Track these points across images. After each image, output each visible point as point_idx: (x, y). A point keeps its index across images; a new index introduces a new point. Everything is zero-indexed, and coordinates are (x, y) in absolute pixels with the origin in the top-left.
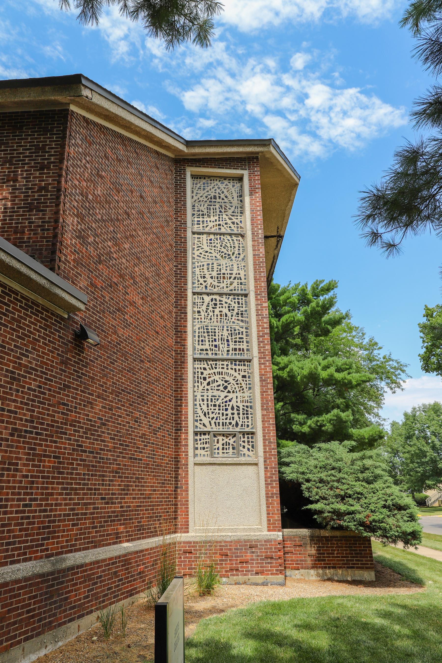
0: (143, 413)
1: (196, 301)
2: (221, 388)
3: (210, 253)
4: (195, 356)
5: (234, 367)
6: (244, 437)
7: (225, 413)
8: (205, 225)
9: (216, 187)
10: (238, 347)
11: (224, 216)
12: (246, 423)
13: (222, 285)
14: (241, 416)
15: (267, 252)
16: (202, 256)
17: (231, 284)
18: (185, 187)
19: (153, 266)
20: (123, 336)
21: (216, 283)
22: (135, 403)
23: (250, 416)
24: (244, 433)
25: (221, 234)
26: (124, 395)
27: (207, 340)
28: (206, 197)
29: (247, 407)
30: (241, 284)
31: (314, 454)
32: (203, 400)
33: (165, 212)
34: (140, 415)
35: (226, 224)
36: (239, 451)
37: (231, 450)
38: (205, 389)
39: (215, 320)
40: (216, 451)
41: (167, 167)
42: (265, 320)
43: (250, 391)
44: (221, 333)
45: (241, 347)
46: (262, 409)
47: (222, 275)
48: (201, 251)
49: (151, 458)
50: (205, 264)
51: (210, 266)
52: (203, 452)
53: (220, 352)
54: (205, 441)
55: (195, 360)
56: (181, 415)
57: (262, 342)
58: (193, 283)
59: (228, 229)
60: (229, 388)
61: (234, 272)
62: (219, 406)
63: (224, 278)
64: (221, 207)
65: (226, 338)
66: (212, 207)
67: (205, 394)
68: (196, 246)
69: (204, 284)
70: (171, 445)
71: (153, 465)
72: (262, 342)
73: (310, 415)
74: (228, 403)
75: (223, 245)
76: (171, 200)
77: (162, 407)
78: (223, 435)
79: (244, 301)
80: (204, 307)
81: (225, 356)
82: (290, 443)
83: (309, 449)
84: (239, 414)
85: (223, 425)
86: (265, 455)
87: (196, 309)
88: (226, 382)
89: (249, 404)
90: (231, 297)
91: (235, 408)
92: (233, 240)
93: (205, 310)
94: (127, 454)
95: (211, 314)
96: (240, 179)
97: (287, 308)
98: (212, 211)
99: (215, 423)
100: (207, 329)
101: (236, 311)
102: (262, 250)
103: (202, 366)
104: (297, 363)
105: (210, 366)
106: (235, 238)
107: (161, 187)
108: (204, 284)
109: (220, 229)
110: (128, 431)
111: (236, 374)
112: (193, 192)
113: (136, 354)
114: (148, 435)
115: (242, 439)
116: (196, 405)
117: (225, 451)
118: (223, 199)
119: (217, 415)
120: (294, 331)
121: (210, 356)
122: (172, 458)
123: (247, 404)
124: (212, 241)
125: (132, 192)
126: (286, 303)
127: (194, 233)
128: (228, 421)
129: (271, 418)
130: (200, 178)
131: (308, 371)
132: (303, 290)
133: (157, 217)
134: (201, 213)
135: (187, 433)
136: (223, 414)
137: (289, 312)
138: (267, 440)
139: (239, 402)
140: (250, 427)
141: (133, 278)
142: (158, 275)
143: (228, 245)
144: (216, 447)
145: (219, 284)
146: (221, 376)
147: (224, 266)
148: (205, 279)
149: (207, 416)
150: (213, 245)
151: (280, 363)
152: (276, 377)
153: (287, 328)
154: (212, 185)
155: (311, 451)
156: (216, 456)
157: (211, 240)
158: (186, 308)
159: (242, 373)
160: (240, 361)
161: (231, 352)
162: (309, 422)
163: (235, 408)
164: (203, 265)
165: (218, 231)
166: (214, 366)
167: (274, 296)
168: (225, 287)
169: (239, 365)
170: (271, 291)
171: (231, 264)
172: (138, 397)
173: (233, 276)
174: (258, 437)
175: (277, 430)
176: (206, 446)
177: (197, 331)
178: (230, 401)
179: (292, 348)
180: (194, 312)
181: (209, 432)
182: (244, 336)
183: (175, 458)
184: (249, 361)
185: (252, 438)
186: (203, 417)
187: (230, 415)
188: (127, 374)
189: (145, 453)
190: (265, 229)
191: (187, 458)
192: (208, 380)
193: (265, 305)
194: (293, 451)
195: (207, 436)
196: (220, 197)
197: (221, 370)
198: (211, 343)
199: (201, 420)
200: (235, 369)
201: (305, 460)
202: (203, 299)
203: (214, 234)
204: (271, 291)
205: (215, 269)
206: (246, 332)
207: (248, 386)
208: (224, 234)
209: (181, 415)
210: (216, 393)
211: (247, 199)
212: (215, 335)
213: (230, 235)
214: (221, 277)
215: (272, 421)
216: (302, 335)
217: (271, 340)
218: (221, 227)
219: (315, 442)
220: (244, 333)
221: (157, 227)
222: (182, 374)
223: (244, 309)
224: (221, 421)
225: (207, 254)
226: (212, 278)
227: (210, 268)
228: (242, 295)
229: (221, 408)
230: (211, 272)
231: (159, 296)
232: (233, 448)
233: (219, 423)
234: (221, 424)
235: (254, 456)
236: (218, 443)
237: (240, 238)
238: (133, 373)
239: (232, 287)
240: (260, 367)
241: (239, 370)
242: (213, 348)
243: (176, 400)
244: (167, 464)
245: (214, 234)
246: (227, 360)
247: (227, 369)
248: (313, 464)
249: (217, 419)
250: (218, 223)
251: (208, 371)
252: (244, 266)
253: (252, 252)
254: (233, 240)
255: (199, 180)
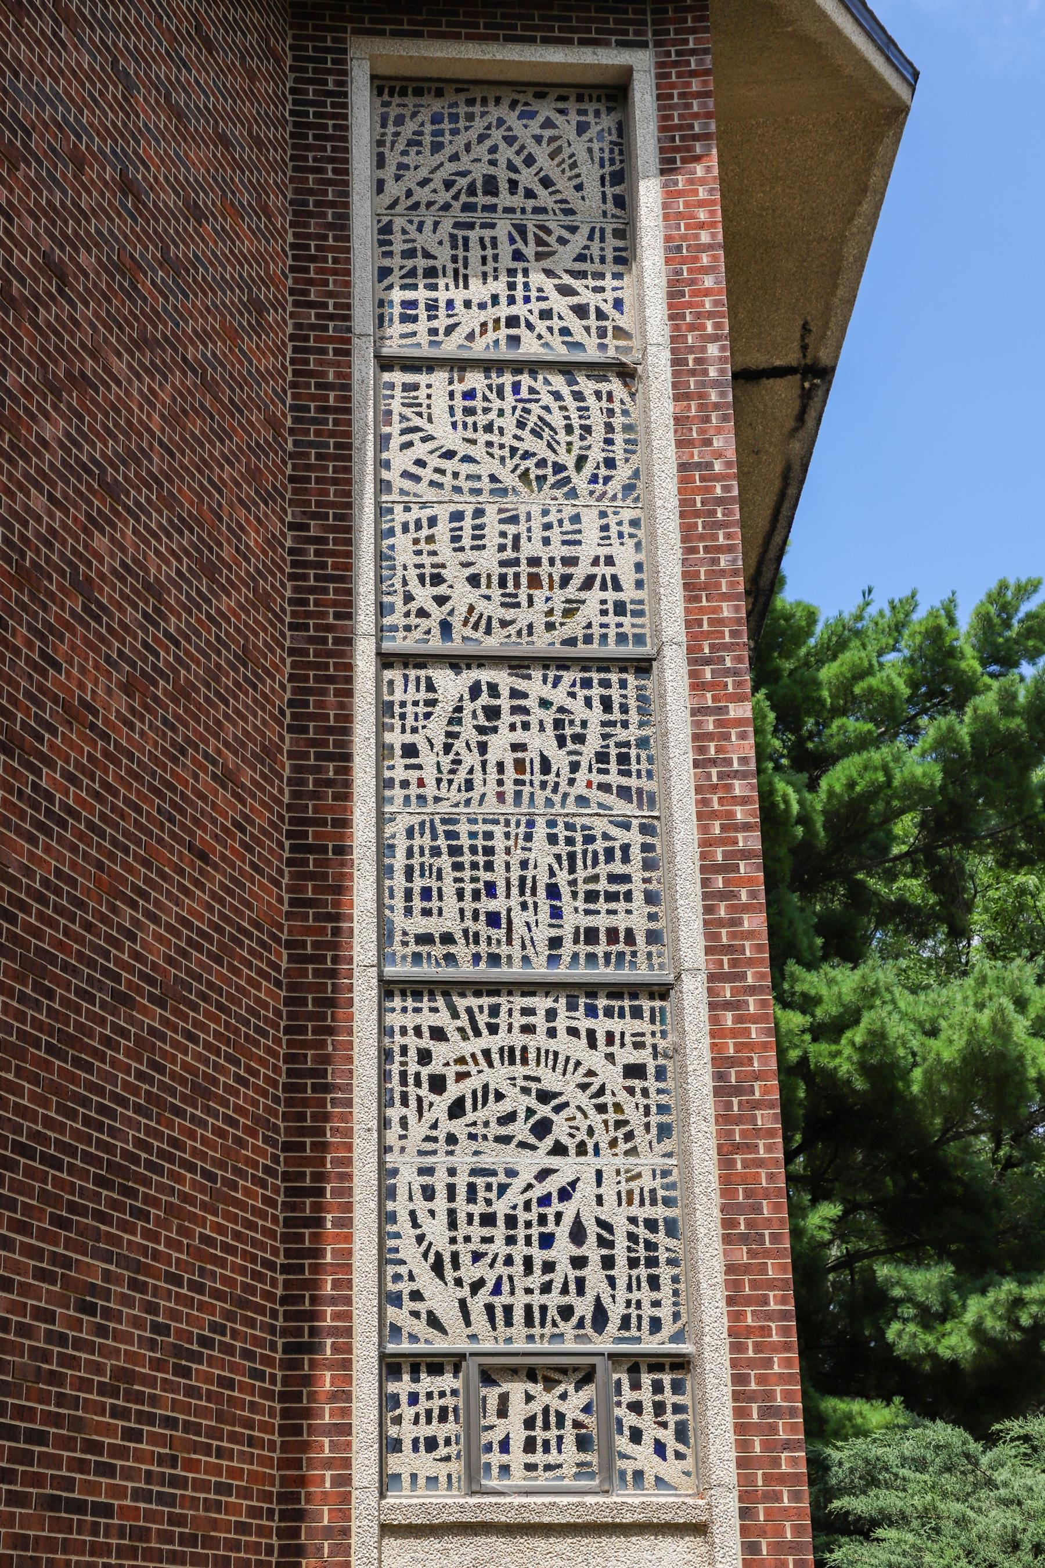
0: (124, 1262)
1: (398, 696)
2: (521, 1129)
3: (467, 459)
4: (391, 971)
5: (584, 1024)
6: (636, 1386)
7: (539, 1256)
8: (441, 323)
9: (497, 135)
10: (602, 922)
11: (537, 279)
12: (647, 1311)
13: (523, 617)
14: (621, 1271)
15: (748, 448)
16: (427, 474)
17: (568, 613)
18: (342, 138)
19: (184, 525)
20: (29, 873)
21: (493, 609)
22: (82, 1211)
23: (665, 1273)
24: (634, 1365)
25: (518, 367)
26: (29, 1172)
27: (449, 888)
28: (448, 185)
29: (651, 1225)
30: (620, 608)
31: (1001, 1475)
32: (429, 1193)
33: (242, 259)
34: (107, 1275)
35: (546, 315)
36: (610, 1455)
37: (570, 1454)
38: (441, 1134)
39: (492, 788)
40: (496, 1458)
41: (253, 38)
42: (739, 788)
43: (667, 1145)
44: (518, 855)
45: (621, 922)
46: (727, 1239)
47: (524, 569)
48: (420, 450)
49: (163, 1499)
50: (443, 513)
51: (468, 523)
52: (425, 1464)
53: (516, 952)
54: (436, 1403)
55: (388, 988)
56: (316, 1269)
57: (723, 896)
58: (382, 610)
59: (556, 341)
60: (560, 1131)
61: (587, 551)
62: (511, 1221)
63: (534, 581)
64: (522, 230)
65: (543, 880)
66: (473, 235)
67: (441, 1161)
68: (395, 429)
69: (437, 613)
70: (265, 1427)
71: (166, 1537)
72: (723, 896)
73: (976, 1269)
74: (556, 1206)
75: (532, 420)
76: (275, 201)
77: (220, 1229)
78: (532, 1375)
79: (631, 692)
80: (436, 728)
81: (540, 970)
82: (876, 1414)
83: (974, 1447)
84: (608, 1262)
85: (529, 1322)
86: (745, 1481)
87: (395, 738)
88: (544, 1097)
89: (660, 1212)
90: (568, 677)
91: (592, 1230)
92: (578, 396)
93: (440, 740)
94: (37, 1480)
95: (471, 759)
96: (616, 93)
97: (854, 725)
98: (475, 253)
99: (490, 1309)
100: (451, 835)
101: (594, 743)
102: (725, 442)
103: (427, 1020)
104: (904, 999)
105: (464, 1021)
106: (587, 386)
107: (224, 140)
108: (437, 613)
109: (514, 341)
110: (46, 1356)
111: (594, 1060)
112: (380, 162)
113: (92, 964)
114: (145, 1380)
115: (628, 1395)
116: (392, 1218)
117: (539, 1457)
118: (530, 194)
119: (500, 1269)
120: (892, 838)
121: (465, 970)
122: (266, 1497)
123: (644, 1213)
124: (478, 403)
125: (79, 163)
126: (847, 701)
127: (386, 364)
128: (554, 1300)
129: (771, 1285)
130: (418, 92)
131: (960, 1041)
132: (935, 635)
133: (205, 288)
134: (421, 263)
135: (347, 1365)
136: (528, 1261)
137: (863, 743)
138: (752, 1397)
139: (610, 1199)
140: (668, 1328)
141: (84, 587)
142: (210, 571)
143: (556, 419)
144: (495, 1437)
145: (509, 614)
146: (519, 1070)
147: (536, 524)
148: (442, 590)
149: (449, 1273)
150: (482, 420)
151: (817, 1000)
152: (793, 1072)
153: (857, 825)
154: (479, 125)
155: (984, 1460)
156: (494, 1482)
157: (469, 395)
158: (347, 731)
159: (627, 1056)
160: (616, 991)
161: (568, 948)
162: (975, 1307)
163: (592, 1230)
164: (433, 521)
165: (505, 353)
166: (482, 1019)
167: (788, 665)
168: (539, 628)
169: (609, 1013)
170: (772, 641)
171: (568, 512)
172: (100, 1181)
173: (580, 573)
174: (711, 1380)
175: (805, 1351)
176: (441, 1431)
177: (401, 844)
178: (565, 1195)
179: (881, 923)
180: (384, 751)
181: (456, 1361)
182: (634, 869)
183: (282, 1498)
184: (662, 991)
185: (678, 1387)
186: (426, 1280)
187: (564, 1268)
188: (48, 1066)
189: (129, 1474)
190: (737, 337)
191: (346, 1498)
192: (453, 1090)
193: (741, 710)
194: (891, 1455)
195: (447, 1381)
196: (513, 185)
197: (518, 1040)
198: (468, 905)
199: (416, 1296)
200: (591, 1034)
201: (956, 1508)
202: (431, 687)
203: (488, 366)
204: (772, 641)
205: (492, 539)
206: (646, 848)
207: (654, 1119)
208: (534, 367)
209: (316, 1269)
210: (495, 1157)
211: (649, 193)
212: (489, 867)
213: (567, 369)
214: (520, 577)
215: (780, 1301)
216: (931, 859)
217: (771, 883)
218: (522, 331)
219: (1015, 1411)
220: (635, 852)
221: (204, 337)
222: (327, 1059)
223: (632, 734)
224: (519, 1301)
225: (449, 465)
226: (474, 580)
227: (467, 533)
228: (623, 664)
229: (521, 1232)
230: (470, 555)
231: (214, 674)
232: (583, 1443)
233: (508, 1310)
234: (519, 1315)
235: (687, 1486)
236: (503, 1412)
237: (615, 385)
238: (77, 1062)
239: (574, 627)
240: (714, 1020)
241: (610, 1038)
242: (481, 926)
243: (289, 1192)
244: (242, 1528)
245: (488, 366)
246: (547, 988)
247: (552, 1033)
248: (995, 1530)
249: (497, 1291)
250: (504, 311)
252: (635, 523)
253: (671, 451)
254: (578, 396)
255: (410, 101)
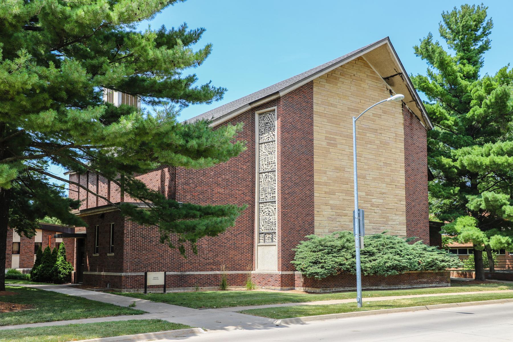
13: (269, 167)
81: (269, 201)
96: (274, 110)
203: (267, 143)
245: (267, 143)
251: (264, 208)
